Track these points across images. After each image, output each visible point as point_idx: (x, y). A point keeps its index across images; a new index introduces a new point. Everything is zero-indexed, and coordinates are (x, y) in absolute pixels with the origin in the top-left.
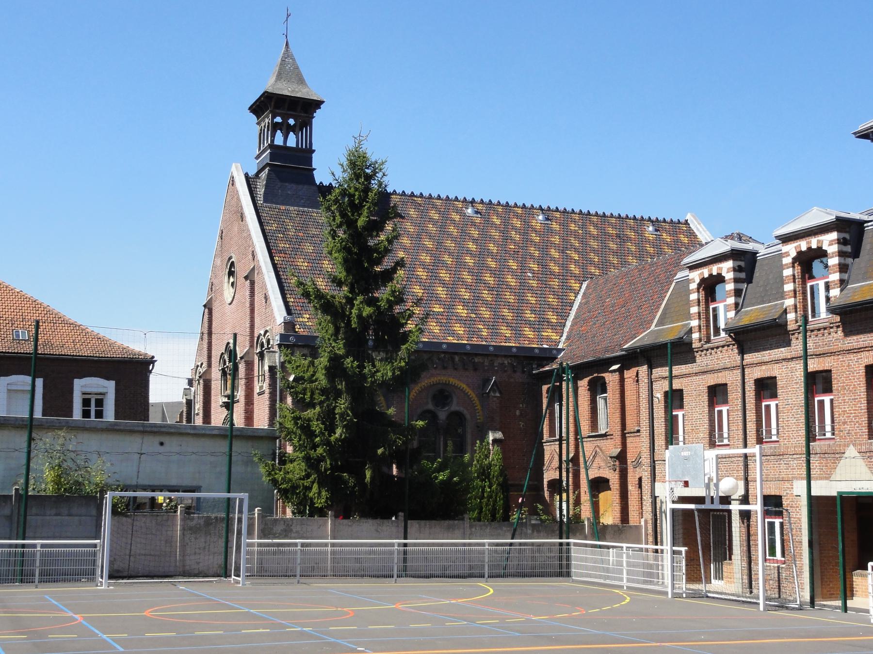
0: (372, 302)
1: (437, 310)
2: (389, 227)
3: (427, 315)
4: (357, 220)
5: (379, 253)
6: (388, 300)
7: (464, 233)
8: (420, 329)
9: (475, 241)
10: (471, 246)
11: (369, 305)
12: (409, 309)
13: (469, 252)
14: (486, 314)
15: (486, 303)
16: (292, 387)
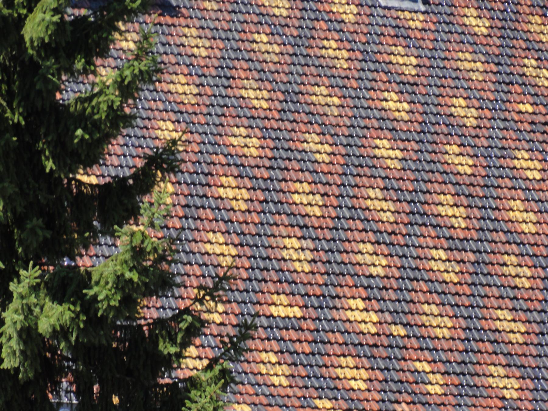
0: (67, 286)
1: (282, 312)
2: (126, 41)
3: (245, 330)
4: (21, 21)
5: (92, 126)
6: (119, 278)
7: (369, 59)
8: (224, 372)
9: (406, 88)
10: (395, 104)
11: (58, 297)
12: (187, 311)
13: (388, 125)
14: (440, 324)
15: (441, 292)
16: (37, 304)
